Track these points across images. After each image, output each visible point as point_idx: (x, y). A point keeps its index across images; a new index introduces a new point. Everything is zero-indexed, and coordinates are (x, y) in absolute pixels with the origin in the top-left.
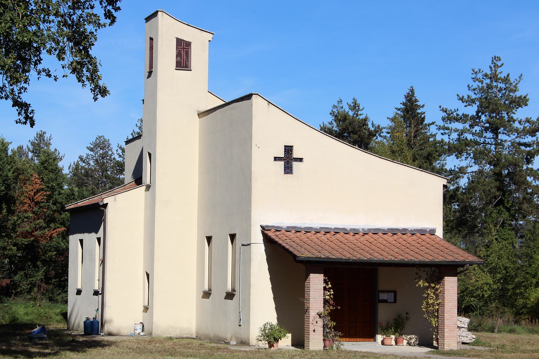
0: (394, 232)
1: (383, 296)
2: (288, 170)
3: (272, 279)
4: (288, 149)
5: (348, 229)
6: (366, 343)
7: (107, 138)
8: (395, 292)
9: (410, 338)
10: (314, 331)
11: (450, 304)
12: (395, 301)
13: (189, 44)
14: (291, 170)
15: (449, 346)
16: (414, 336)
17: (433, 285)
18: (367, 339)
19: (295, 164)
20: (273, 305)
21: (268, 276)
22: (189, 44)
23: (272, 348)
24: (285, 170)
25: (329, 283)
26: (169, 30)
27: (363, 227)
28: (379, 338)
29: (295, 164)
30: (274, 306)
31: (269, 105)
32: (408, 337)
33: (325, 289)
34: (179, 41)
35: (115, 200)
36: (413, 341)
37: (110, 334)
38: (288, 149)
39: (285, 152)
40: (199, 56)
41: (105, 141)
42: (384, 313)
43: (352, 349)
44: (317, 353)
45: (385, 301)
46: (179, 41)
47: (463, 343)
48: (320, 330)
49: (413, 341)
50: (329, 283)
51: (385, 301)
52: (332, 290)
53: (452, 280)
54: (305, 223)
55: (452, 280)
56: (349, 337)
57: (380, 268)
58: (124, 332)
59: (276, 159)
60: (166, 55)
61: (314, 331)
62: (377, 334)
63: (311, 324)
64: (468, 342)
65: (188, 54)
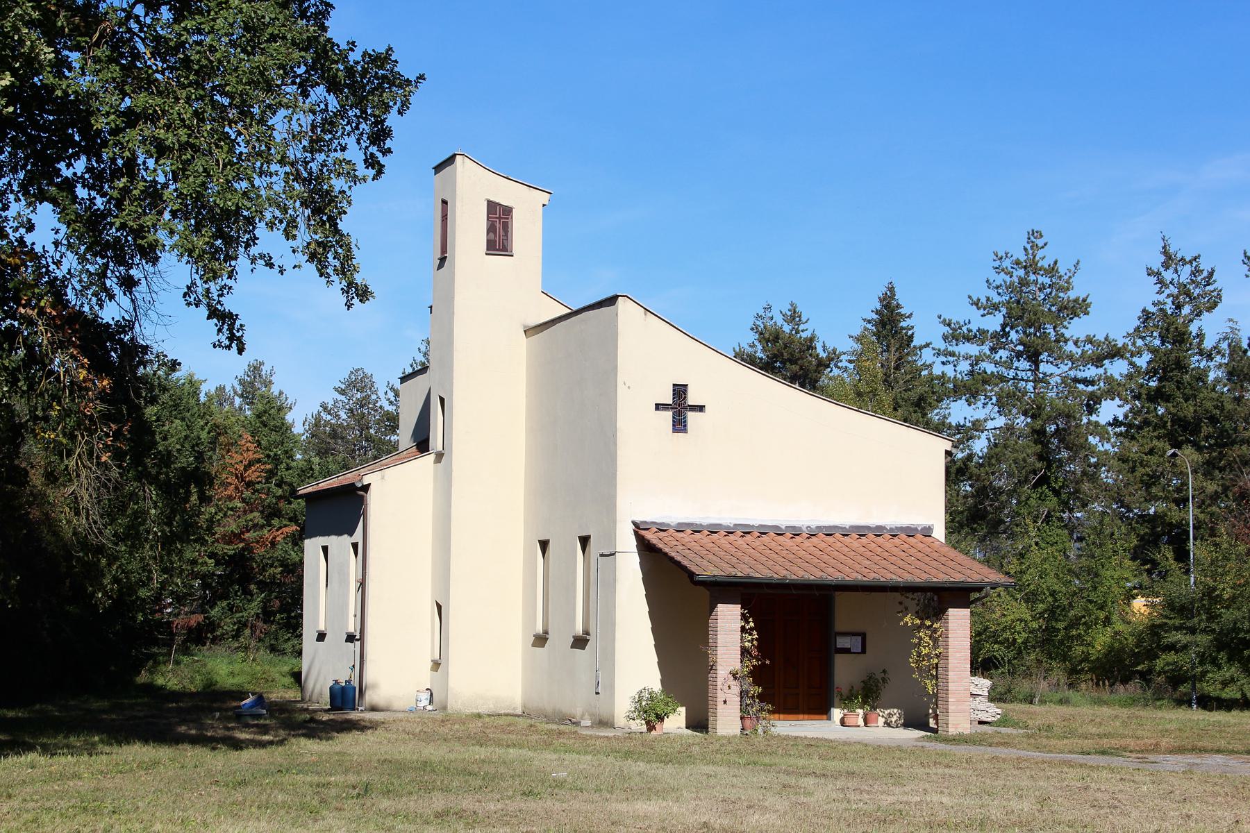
1: (842, 642)
2: (680, 425)
4: (680, 391)
7: (368, 371)
13: (508, 211)
17: (928, 623)
19: (691, 416)
22: (508, 211)
23: (653, 733)
26: (474, 187)
28: (837, 713)
29: (691, 416)
33: (743, 629)
35: (383, 478)
37: (374, 709)
38: (680, 391)
42: (845, 671)
45: (847, 651)
47: (980, 723)
51: (847, 651)
56: (809, 713)
58: (398, 704)
59: (658, 407)
60: (470, 229)
64: (989, 720)
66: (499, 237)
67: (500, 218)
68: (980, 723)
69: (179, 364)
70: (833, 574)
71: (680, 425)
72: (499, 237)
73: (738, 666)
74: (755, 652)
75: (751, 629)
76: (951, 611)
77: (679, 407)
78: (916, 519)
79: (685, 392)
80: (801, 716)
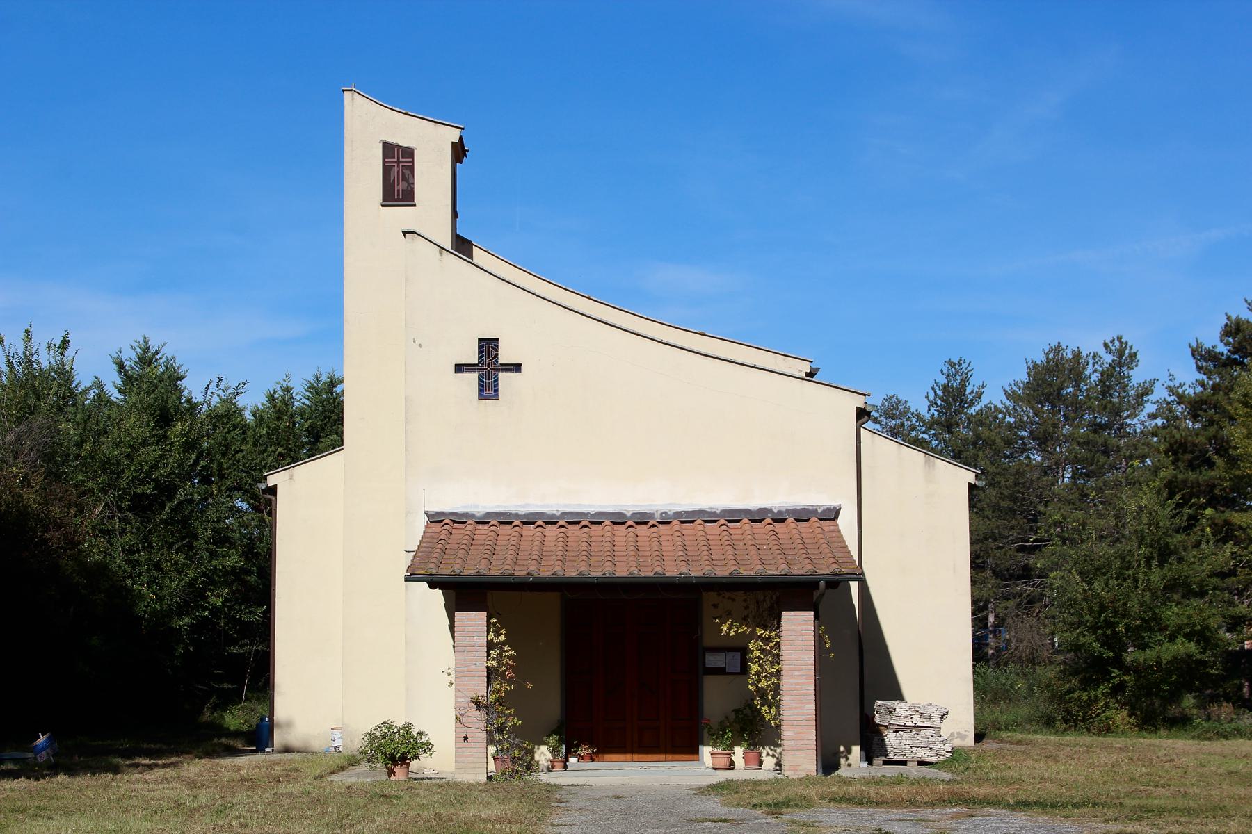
0: (733, 517)
1: (713, 660)
2: (488, 389)
4: (488, 347)
5: (629, 515)
6: (675, 764)
7: (902, 397)
11: (796, 673)
13: (409, 153)
14: (497, 390)
15: (795, 770)
17: (760, 631)
18: (621, 757)
19: (504, 378)
22: (409, 153)
23: (393, 778)
24: (481, 390)
25: (503, 631)
26: (368, 124)
27: (665, 509)
28: (706, 751)
29: (504, 378)
33: (490, 645)
35: (291, 477)
37: (287, 750)
38: (488, 347)
39: (481, 352)
40: (432, 174)
41: (899, 402)
42: (716, 698)
43: (33, 784)
45: (720, 671)
47: (921, 763)
50: (503, 631)
51: (720, 671)
53: (801, 618)
54: (527, 505)
55: (801, 618)
56: (639, 752)
57: (489, 594)
58: (317, 744)
59: (460, 368)
60: (363, 175)
62: (703, 744)
64: (934, 759)
66: (398, 182)
67: (398, 162)
68: (921, 763)
69: (147, 358)
70: (699, 569)
71: (488, 389)
72: (398, 182)
73: (481, 690)
74: (509, 674)
75: (503, 644)
76: (786, 615)
77: (488, 367)
78: (821, 500)
79: (496, 348)
80: (663, 757)
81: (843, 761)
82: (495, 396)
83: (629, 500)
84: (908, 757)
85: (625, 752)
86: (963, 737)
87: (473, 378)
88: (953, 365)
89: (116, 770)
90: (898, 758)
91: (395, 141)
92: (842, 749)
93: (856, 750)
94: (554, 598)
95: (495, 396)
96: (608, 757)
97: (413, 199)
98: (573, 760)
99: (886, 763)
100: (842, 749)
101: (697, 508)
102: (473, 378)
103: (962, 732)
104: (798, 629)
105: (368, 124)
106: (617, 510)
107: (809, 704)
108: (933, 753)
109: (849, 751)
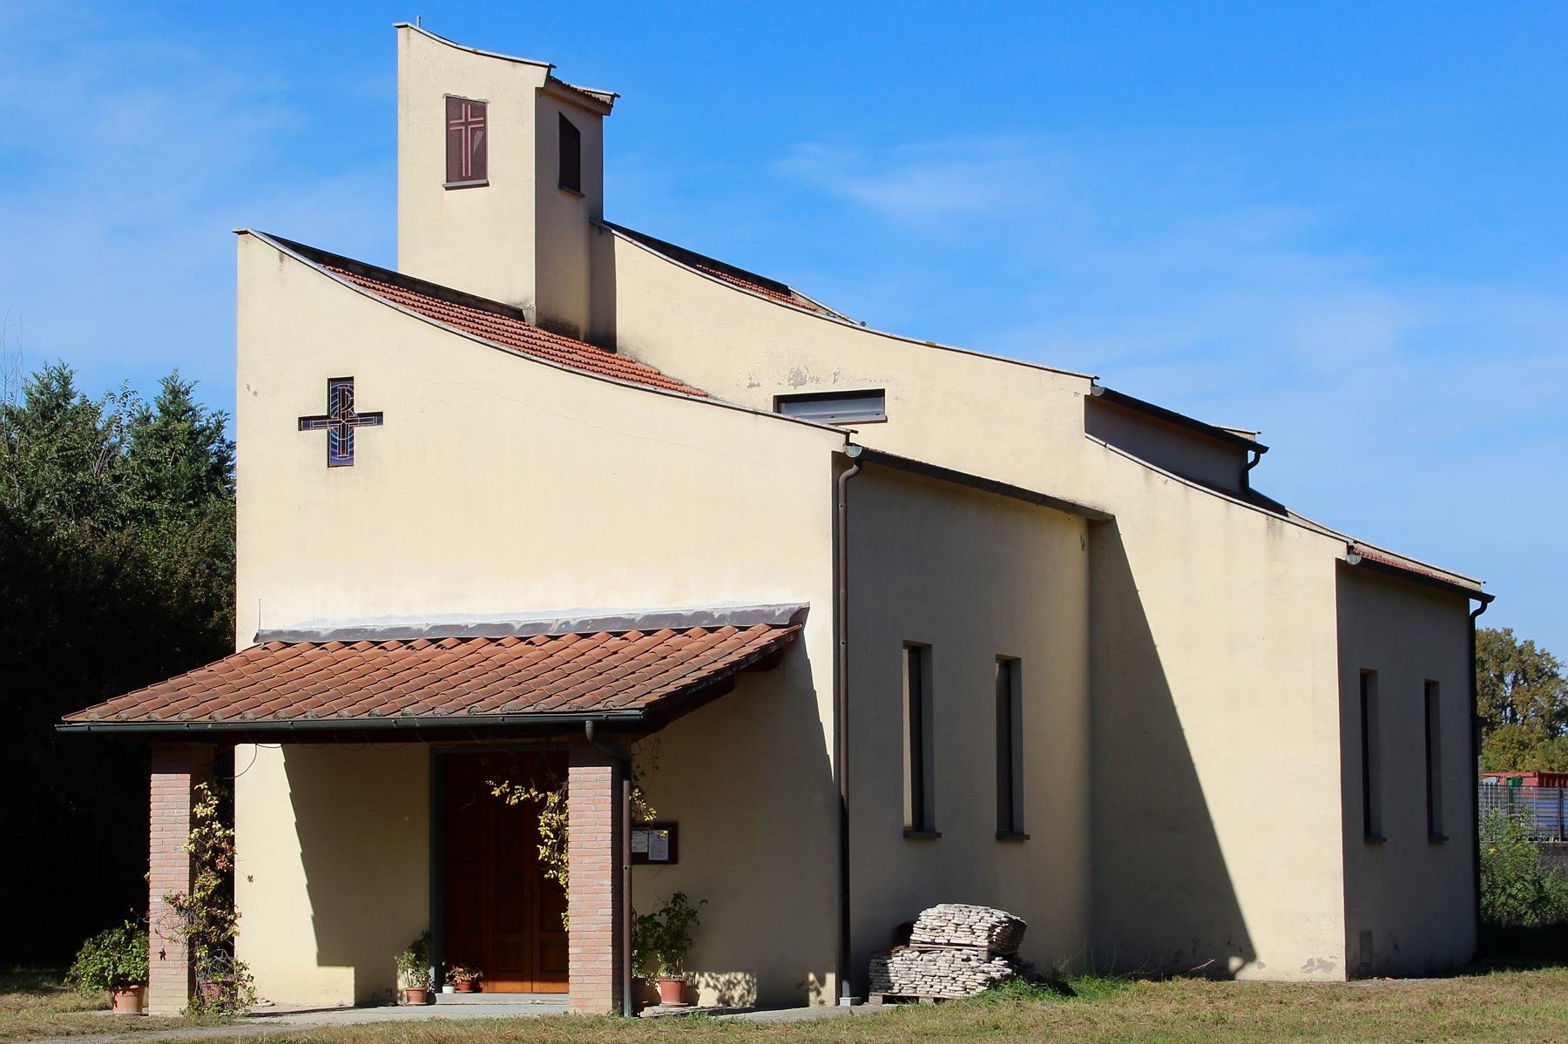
2: (340, 452)
3: (295, 797)
4: (340, 390)
8: (673, 828)
9: (729, 982)
10: (163, 954)
11: (586, 860)
12: (673, 858)
13: (479, 109)
16: (740, 976)
18: (517, 986)
19: (360, 432)
20: (302, 879)
21: (286, 789)
22: (479, 109)
30: (305, 881)
31: (281, 259)
32: (723, 978)
34: (454, 104)
36: (737, 993)
38: (340, 390)
44: (171, 1024)
46: (454, 104)
48: (179, 952)
49: (737, 993)
52: (543, 831)
53: (594, 777)
54: (389, 617)
56: (542, 980)
60: (423, 142)
61: (163, 954)
63: (152, 934)
65: (453, 141)
81: (812, 996)
82: (349, 462)
83: (689, 602)
84: (920, 993)
85: (522, 979)
86: (1327, 967)
87: (320, 436)
88: (175, 393)
89: (48, 991)
90: (906, 993)
91: (461, 95)
92: (812, 977)
93: (831, 978)
94: (421, 750)
95: (349, 462)
96: (500, 985)
97: (485, 177)
98: (447, 989)
99: (887, 1000)
100: (812, 977)
101: (611, 615)
102: (320, 436)
103: (1326, 959)
104: (590, 789)
105: (429, 71)
106: (505, 620)
107: (603, 906)
108: (958, 986)
109: (822, 981)
